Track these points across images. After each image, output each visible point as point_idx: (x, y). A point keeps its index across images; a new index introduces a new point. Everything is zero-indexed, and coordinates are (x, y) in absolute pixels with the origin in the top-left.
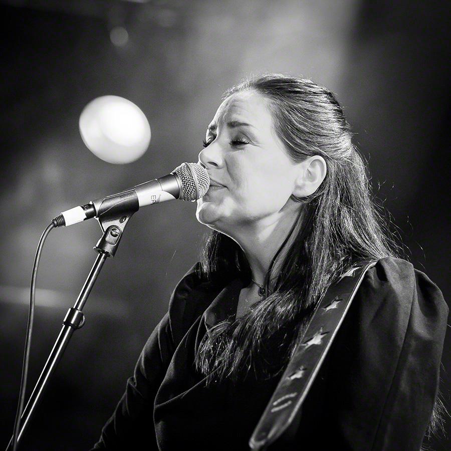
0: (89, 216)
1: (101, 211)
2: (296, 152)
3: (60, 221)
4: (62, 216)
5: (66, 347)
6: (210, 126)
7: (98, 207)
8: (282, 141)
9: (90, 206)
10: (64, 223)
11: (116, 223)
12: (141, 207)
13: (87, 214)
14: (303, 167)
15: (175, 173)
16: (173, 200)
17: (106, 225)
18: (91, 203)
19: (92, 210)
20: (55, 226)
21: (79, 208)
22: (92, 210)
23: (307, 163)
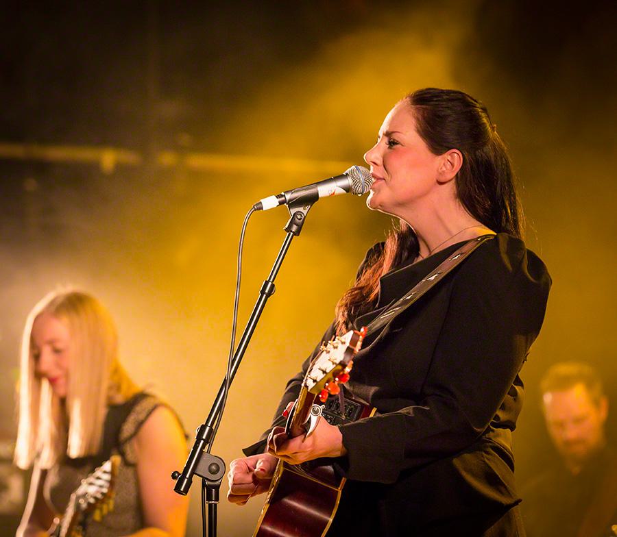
0: (281, 203)
1: (290, 200)
2: (448, 107)
3: (259, 206)
4: (261, 203)
5: (335, 178)
6: (381, 134)
7: (288, 197)
8: (386, 322)
9: (282, 196)
10: (262, 209)
11: (301, 209)
12: (322, 198)
13: (279, 202)
14: (444, 158)
15: (347, 174)
16: (343, 195)
17: (293, 211)
18: (283, 193)
19: (283, 198)
20: (255, 210)
21: (274, 197)
22: (283, 198)
23: (447, 156)
